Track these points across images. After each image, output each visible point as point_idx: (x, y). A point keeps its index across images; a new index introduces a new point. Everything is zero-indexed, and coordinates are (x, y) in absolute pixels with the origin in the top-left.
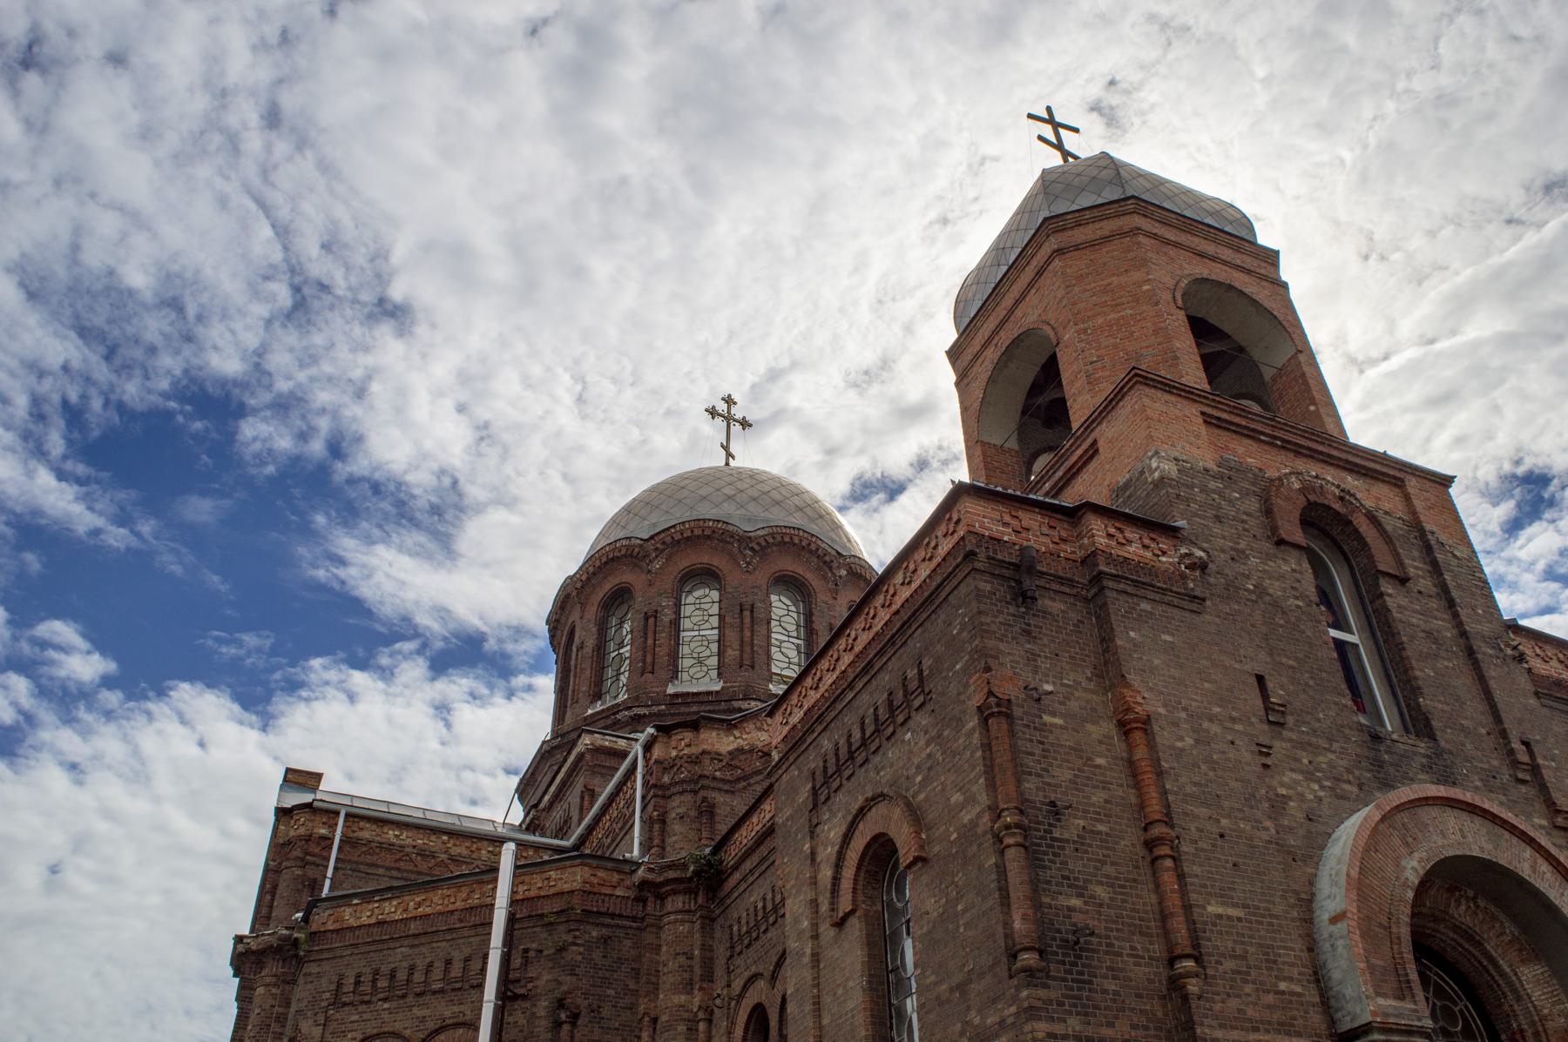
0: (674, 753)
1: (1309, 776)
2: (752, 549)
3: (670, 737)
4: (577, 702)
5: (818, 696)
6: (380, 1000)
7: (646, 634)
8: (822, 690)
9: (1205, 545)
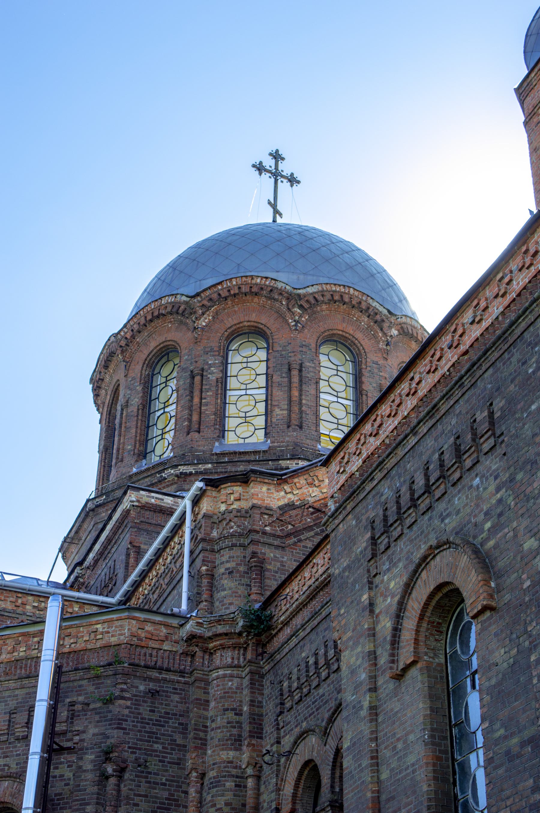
0: (223, 508)
2: (301, 307)
3: (219, 491)
5: (378, 443)
8: (383, 435)
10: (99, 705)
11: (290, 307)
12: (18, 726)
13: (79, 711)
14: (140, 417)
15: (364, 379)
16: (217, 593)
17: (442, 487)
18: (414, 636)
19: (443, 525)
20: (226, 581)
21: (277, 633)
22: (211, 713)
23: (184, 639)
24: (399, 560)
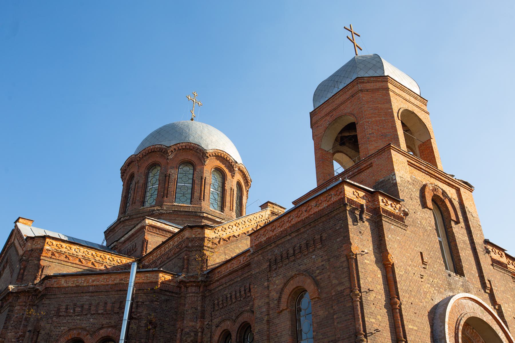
0: (194, 236)
1: (432, 286)
3: (192, 230)
4: (135, 203)
5: (273, 234)
6: (76, 315)
7: (165, 182)
8: (275, 232)
9: (408, 207)
10: (148, 303)
11: (204, 156)
12: (115, 308)
13: (140, 305)
14: (143, 188)
15: (226, 185)
16: (190, 266)
17: (300, 255)
18: (287, 301)
19: (299, 267)
20: (194, 263)
21: (213, 283)
22: (186, 309)
23: (178, 281)
24: (280, 274)
